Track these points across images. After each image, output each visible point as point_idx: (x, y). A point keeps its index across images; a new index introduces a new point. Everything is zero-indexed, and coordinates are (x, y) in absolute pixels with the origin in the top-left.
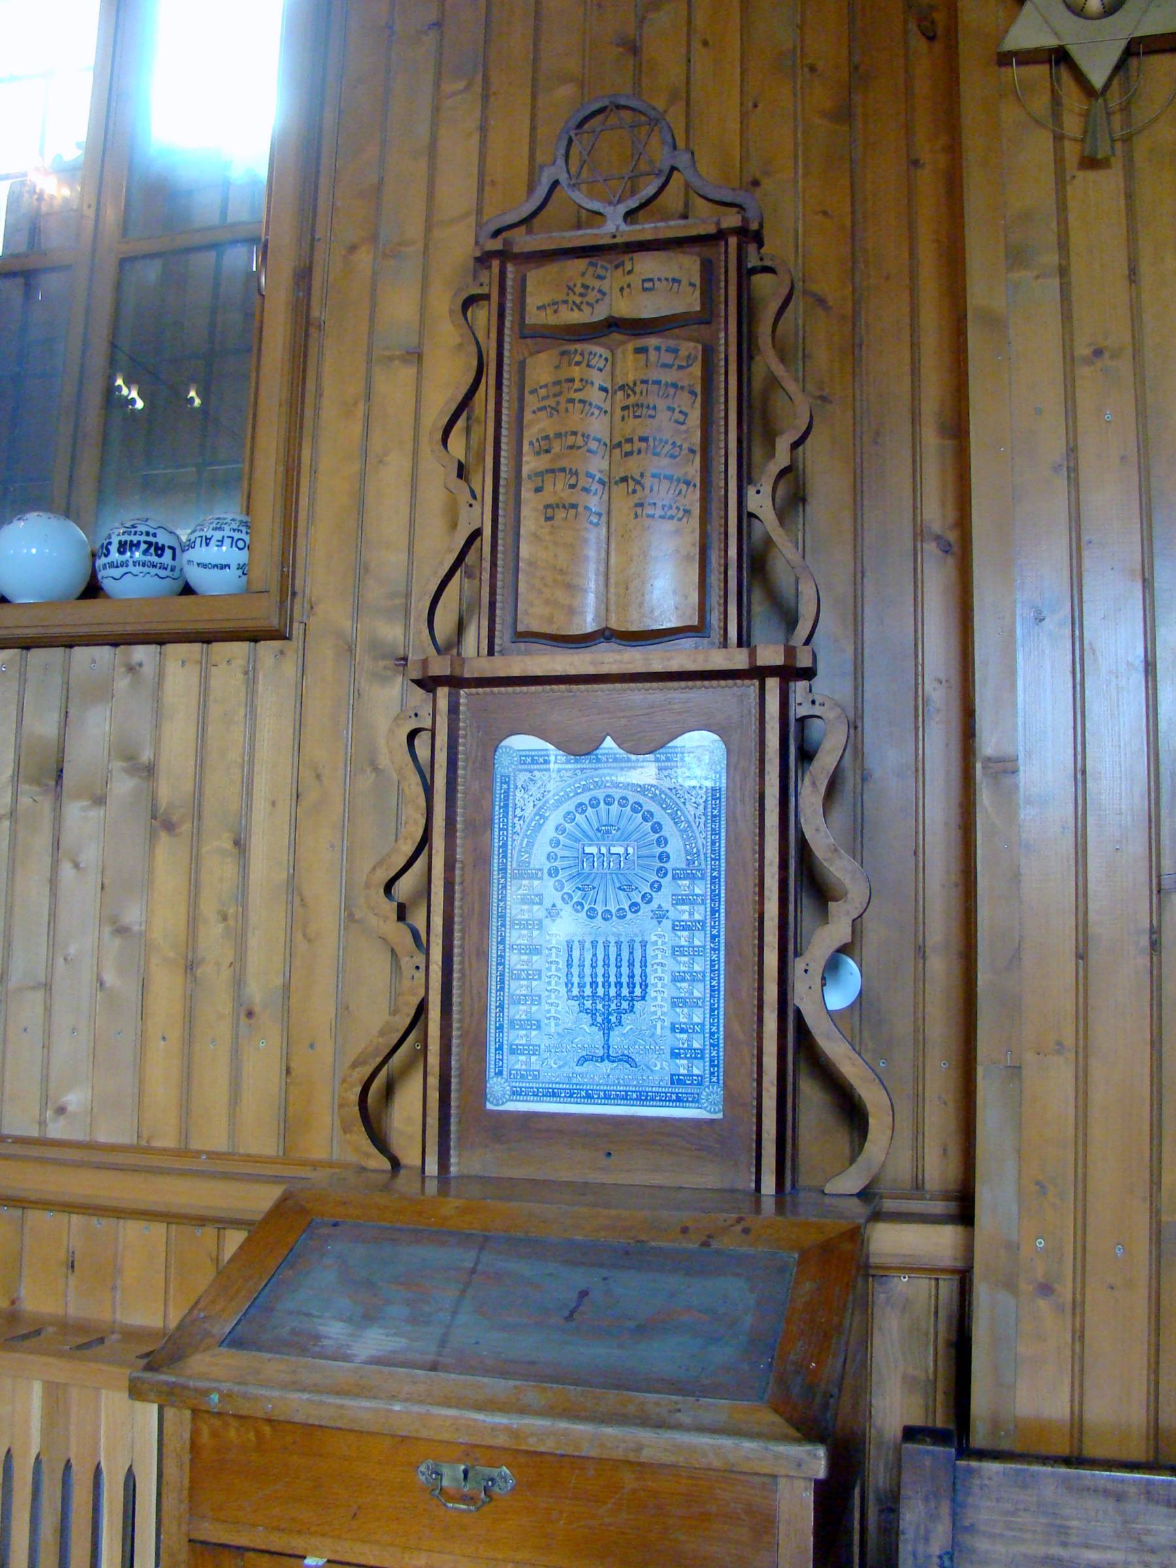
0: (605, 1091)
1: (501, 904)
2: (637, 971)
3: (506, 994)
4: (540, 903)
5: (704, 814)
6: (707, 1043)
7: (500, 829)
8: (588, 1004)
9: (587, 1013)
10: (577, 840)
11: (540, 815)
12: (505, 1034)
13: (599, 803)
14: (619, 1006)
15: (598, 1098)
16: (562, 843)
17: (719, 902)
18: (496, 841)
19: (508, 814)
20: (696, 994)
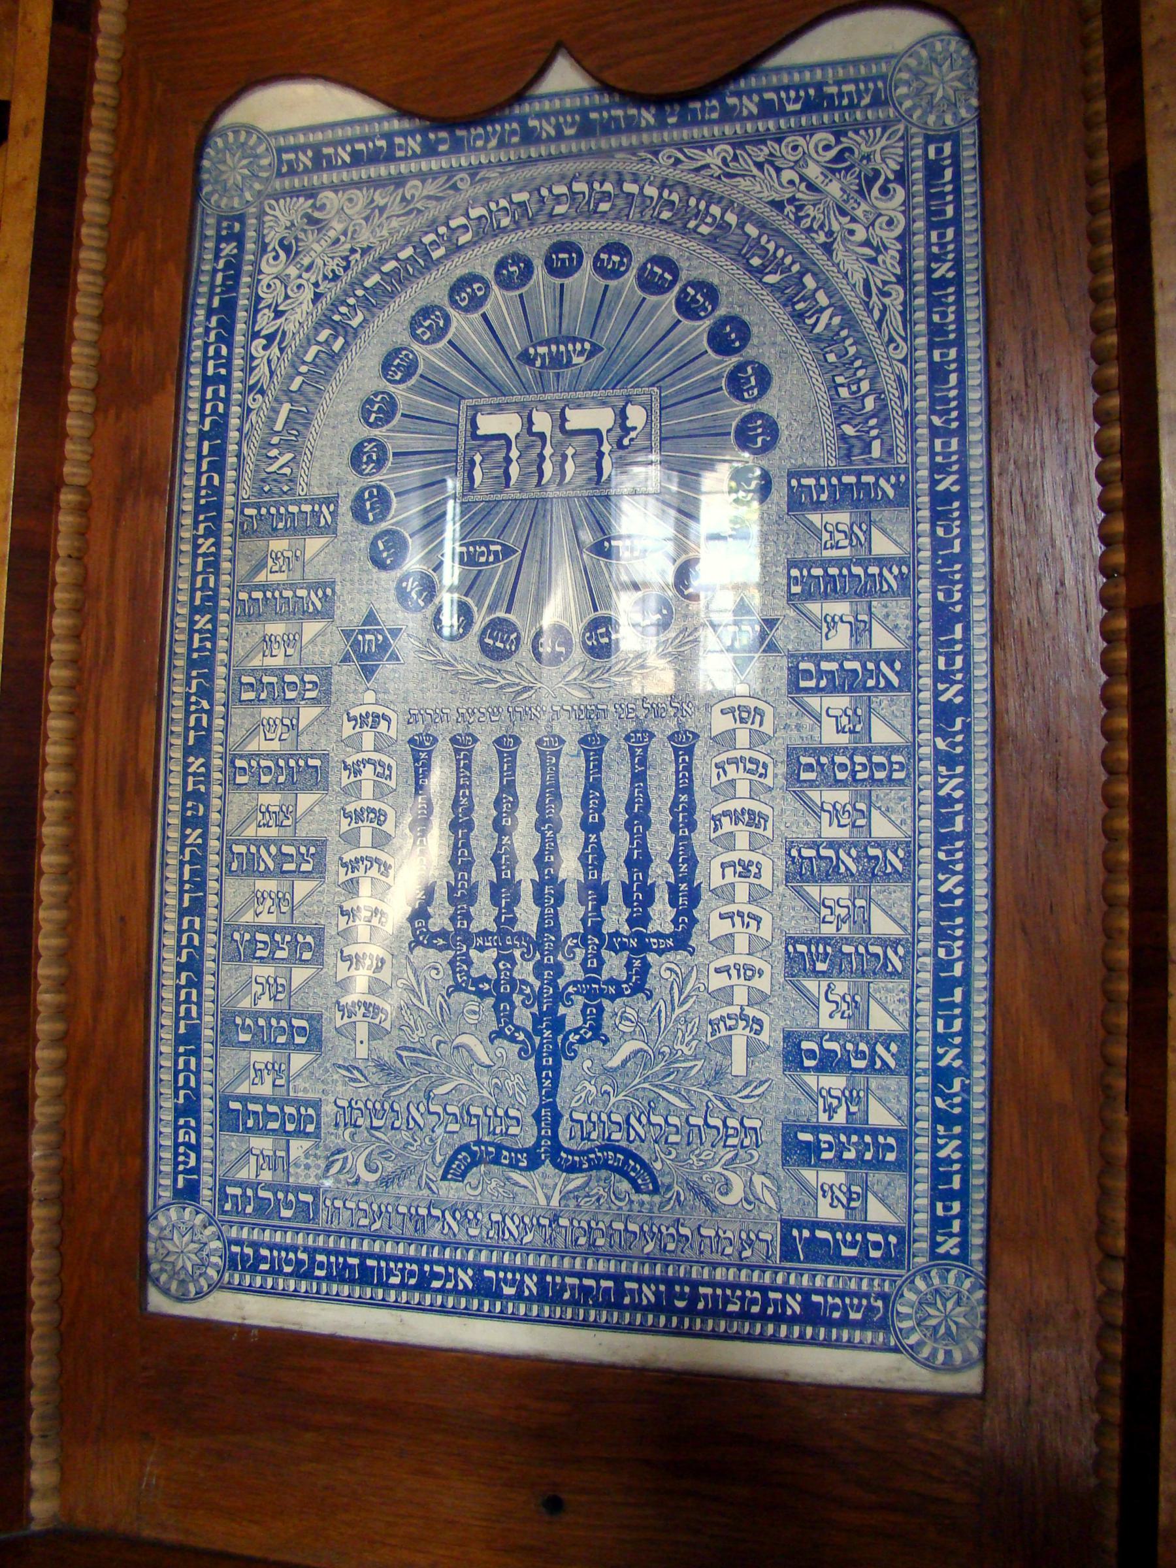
0: (542, 1273)
1: (202, 622)
2: (661, 842)
3: (211, 924)
4: (326, 614)
5: (901, 280)
6: (924, 1110)
7: (206, 381)
8: (484, 962)
9: (482, 994)
10: (453, 396)
11: (334, 325)
12: (207, 1061)
13: (529, 269)
14: (592, 969)
15: (519, 1296)
16: (401, 409)
17: (967, 582)
18: (193, 417)
19: (231, 330)
20: (882, 925)
